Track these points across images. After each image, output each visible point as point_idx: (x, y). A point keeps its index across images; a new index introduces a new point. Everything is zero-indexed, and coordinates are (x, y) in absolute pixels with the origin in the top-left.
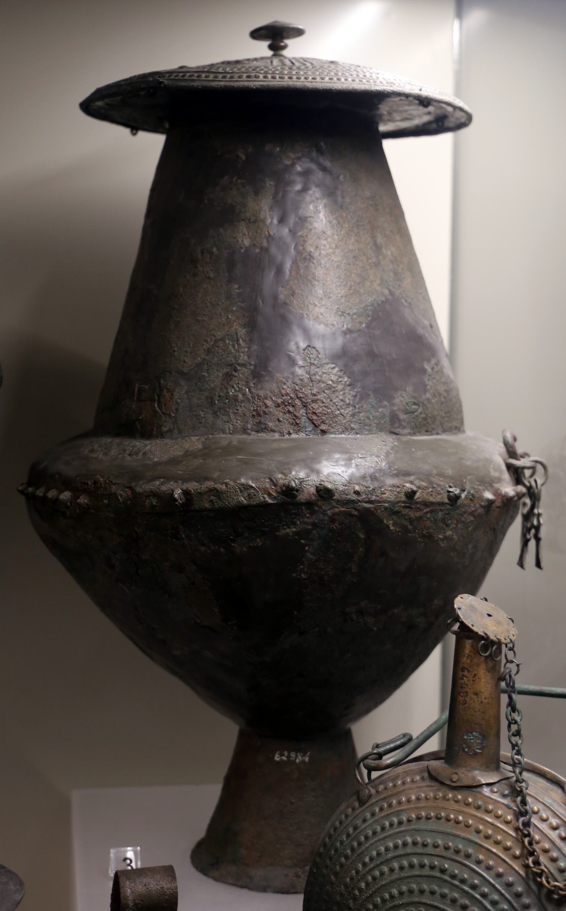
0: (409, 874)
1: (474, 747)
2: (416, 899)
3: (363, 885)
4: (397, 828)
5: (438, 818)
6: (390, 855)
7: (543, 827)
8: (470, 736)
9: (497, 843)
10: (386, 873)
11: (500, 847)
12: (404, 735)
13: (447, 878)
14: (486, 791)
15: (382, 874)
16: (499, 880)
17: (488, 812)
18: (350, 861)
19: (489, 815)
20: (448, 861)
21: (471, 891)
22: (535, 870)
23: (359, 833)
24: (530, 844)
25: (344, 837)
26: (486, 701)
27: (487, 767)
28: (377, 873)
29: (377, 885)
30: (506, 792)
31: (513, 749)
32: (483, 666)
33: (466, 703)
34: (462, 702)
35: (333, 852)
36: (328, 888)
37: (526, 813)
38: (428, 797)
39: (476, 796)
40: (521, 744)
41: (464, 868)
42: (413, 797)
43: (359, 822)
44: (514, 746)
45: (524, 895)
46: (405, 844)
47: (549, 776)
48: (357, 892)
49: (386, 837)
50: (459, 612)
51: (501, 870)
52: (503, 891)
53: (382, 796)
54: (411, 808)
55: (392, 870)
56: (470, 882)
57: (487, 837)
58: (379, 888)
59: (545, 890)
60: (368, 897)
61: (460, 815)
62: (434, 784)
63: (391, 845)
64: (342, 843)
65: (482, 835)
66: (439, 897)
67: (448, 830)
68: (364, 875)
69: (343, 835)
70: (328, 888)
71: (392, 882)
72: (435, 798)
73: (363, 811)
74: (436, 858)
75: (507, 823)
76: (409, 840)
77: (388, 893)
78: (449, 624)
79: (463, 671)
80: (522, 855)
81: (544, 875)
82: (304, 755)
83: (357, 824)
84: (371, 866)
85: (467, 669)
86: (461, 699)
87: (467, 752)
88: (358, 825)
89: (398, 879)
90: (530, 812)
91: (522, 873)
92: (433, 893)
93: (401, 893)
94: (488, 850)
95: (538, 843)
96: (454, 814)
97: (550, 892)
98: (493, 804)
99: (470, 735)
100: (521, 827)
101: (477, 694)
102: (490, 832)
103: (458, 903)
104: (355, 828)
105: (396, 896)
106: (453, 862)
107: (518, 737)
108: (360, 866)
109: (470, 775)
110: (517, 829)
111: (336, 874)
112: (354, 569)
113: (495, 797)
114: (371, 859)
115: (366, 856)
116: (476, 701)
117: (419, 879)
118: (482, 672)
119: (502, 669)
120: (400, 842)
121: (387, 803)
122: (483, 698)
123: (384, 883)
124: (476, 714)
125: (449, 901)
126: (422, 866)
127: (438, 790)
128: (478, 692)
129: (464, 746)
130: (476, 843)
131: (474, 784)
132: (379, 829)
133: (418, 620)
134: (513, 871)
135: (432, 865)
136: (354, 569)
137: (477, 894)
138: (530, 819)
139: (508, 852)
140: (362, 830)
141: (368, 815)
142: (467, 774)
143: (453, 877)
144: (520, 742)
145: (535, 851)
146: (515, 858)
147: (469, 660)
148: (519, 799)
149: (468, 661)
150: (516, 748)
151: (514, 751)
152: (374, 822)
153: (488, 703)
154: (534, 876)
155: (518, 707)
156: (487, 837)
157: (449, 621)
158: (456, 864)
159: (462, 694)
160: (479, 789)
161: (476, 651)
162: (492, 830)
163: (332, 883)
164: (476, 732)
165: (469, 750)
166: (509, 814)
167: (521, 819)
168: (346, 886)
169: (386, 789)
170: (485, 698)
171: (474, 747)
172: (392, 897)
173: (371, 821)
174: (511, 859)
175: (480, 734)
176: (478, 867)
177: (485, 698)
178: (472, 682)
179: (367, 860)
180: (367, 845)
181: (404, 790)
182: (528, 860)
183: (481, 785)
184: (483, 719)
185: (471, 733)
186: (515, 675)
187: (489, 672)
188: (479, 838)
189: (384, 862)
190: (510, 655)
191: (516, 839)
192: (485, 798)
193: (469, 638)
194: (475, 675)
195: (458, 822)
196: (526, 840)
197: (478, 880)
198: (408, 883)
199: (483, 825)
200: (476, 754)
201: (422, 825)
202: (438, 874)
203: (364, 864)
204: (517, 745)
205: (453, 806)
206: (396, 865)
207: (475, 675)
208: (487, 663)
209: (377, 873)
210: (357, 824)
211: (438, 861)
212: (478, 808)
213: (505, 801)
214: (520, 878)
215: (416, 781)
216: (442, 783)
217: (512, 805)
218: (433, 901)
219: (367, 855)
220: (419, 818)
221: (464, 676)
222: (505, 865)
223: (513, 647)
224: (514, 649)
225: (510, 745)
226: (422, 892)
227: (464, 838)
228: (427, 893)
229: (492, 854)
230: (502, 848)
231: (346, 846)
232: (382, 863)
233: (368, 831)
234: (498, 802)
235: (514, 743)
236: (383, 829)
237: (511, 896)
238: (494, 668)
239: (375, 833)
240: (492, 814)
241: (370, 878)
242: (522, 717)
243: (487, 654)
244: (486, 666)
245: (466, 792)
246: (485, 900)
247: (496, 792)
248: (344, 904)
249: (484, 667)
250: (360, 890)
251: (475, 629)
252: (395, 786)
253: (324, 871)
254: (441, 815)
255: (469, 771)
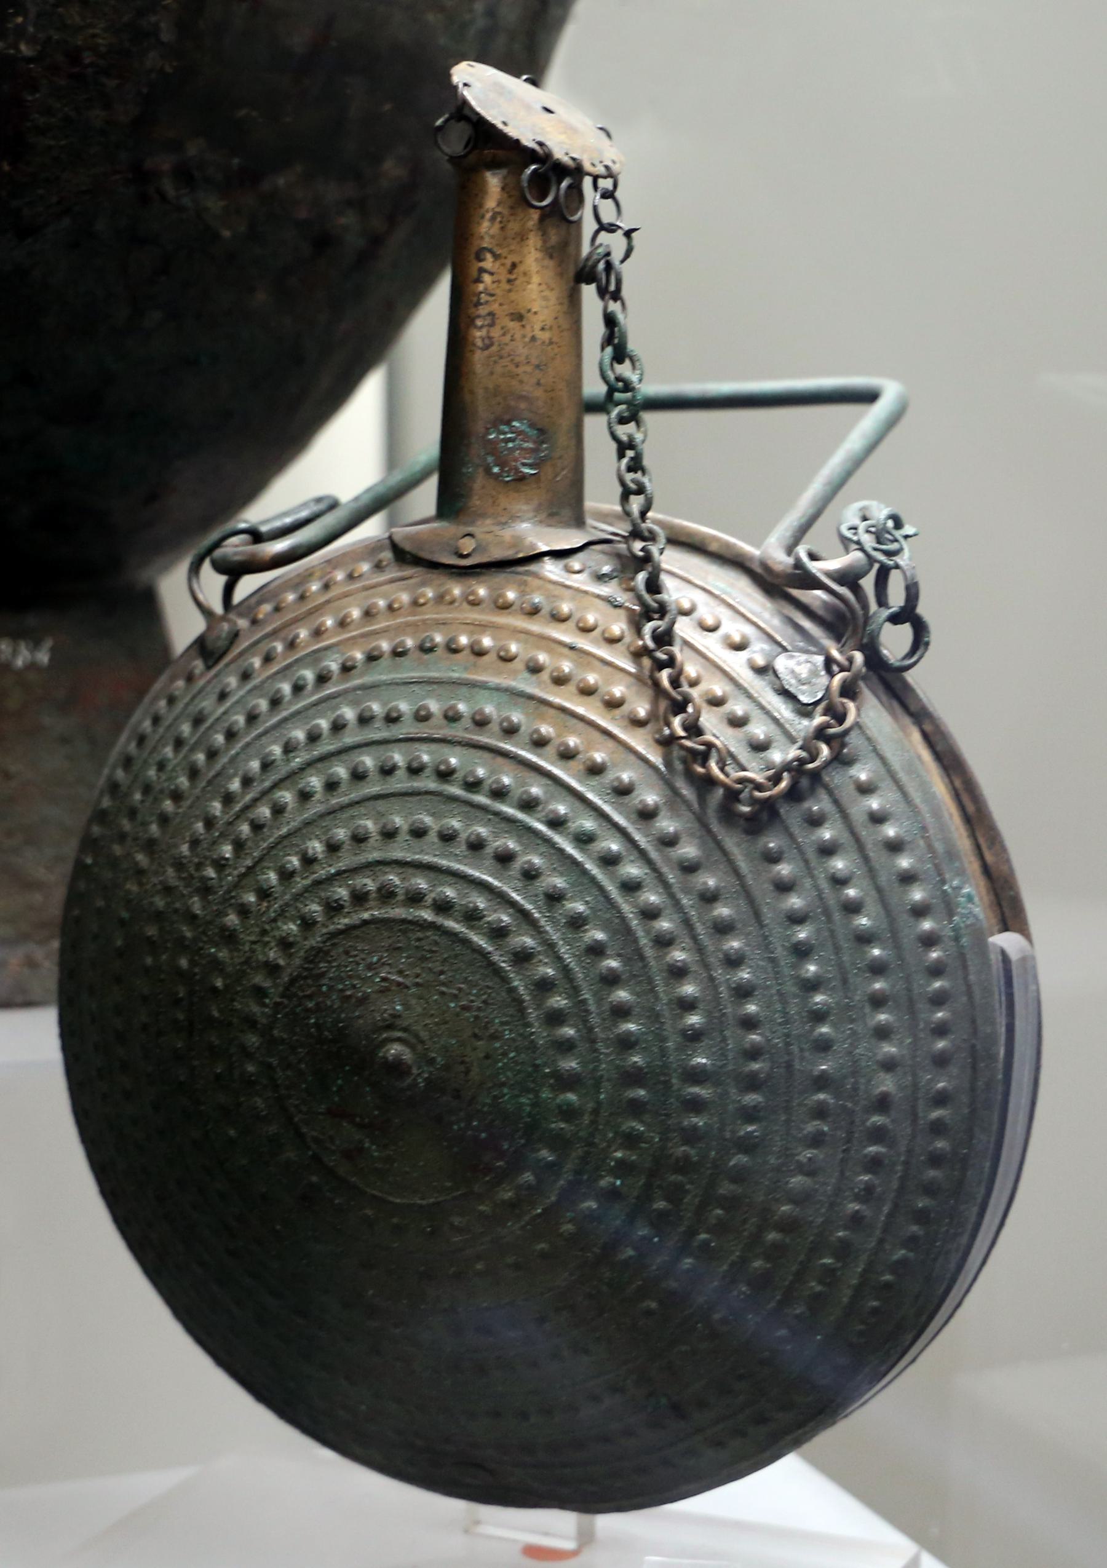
0: (354, 796)
1: (516, 460)
2: (375, 855)
3: (227, 851)
4: (312, 694)
5: (426, 649)
6: (297, 761)
7: (710, 644)
8: (505, 433)
9: (587, 692)
10: (289, 808)
11: (594, 701)
12: (319, 500)
13: (455, 790)
14: (551, 569)
15: (278, 810)
16: (595, 781)
17: (559, 619)
18: (186, 803)
19: (563, 626)
20: (458, 749)
21: (520, 815)
22: (688, 743)
23: (209, 728)
24: (675, 682)
25: (168, 751)
26: (545, 336)
27: (552, 515)
28: (264, 812)
29: (264, 840)
30: (606, 569)
31: (621, 455)
32: (534, 241)
33: (492, 344)
34: (479, 343)
35: (138, 796)
36: (132, 887)
37: (662, 610)
38: (396, 606)
39: (525, 583)
40: (643, 441)
41: (500, 760)
42: (356, 613)
43: (207, 703)
44: (623, 447)
45: (663, 813)
46: (338, 727)
47: (713, 547)
48: (211, 872)
49: (285, 720)
50: (467, 93)
51: (599, 757)
52: (607, 808)
53: (269, 629)
54: (353, 638)
55: (305, 796)
56: (517, 793)
57: (560, 681)
58: (271, 848)
59: (720, 792)
60: (242, 876)
61: (483, 632)
62: (409, 571)
63: (300, 735)
64: (161, 766)
65: (545, 676)
66: (436, 840)
67: (456, 675)
68: (230, 824)
69: (164, 746)
70: (132, 887)
71: (308, 824)
72: (415, 603)
73: (216, 676)
74: (424, 747)
75: (612, 641)
76: (349, 714)
77: (296, 854)
78: (440, 128)
79: (479, 258)
80: (653, 716)
81: (714, 755)
82: (36, 644)
83: (201, 712)
84: (248, 798)
85: (490, 251)
86: (478, 335)
87: (496, 477)
88: (206, 712)
89: (322, 816)
90: (672, 608)
91: (655, 757)
92: (419, 833)
93: (333, 848)
94: (563, 710)
95: (693, 684)
96: (471, 634)
97: (732, 795)
98: (573, 599)
99: (505, 428)
100: (651, 644)
101: (519, 317)
102: (566, 667)
103: (489, 850)
104: (198, 721)
105: (320, 856)
106: (472, 751)
107: (633, 424)
108: (216, 807)
109: (507, 534)
110: (638, 655)
111: (150, 846)
112: (167, 35)
113: (580, 581)
114: (247, 782)
115: (230, 778)
116: (518, 336)
117: (381, 805)
118: (532, 257)
119: (586, 249)
120: (324, 724)
121: (284, 640)
122: (537, 327)
123: (284, 830)
124: (520, 370)
125: (464, 847)
126: (388, 771)
127: (423, 584)
128: (523, 312)
129: (490, 459)
130: (531, 697)
131: (521, 555)
132: (263, 705)
133: (343, 221)
134: (632, 758)
135: (415, 765)
136: (167, 35)
137: (539, 820)
138: (673, 623)
139: (617, 712)
140: (218, 719)
141: (233, 681)
142: (500, 533)
143: (474, 785)
144: (639, 437)
145: (687, 700)
146: (637, 723)
147: (497, 226)
148: (641, 577)
149: (495, 229)
150: (630, 453)
151: (625, 461)
152: (250, 691)
153: (551, 343)
154: (689, 761)
155: (632, 346)
156: (560, 681)
157: (439, 122)
158: (480, 753)
159: (479, 323)
160: (533, 567)
161: (518, 200)
162: (573, 661)
163: (140, 872)
164: (520, 420)
165: (502, 470)
166: (616, 620)
167: (648, 628)
168: (179, 865)
169: (277, 609)
170: (543, 329)
171: (516, 460)
172: (308, 861)
173: (242, 693)
174: (624, 728)
175: (532, 425)
176: (539, 756)
177: (543, 329)
178: (507, 287)
179: (235, 785)
180: (233, 752)
181: (328, 602)
182: (668, 724)
183: (539, 557)
184: (538, 384)
185: (508, 423)
186: (622, 262)
187: (551, 257)
188: (539, 684)
189: (282, 780)
190: (608, 212)
191: (638, 678)
192: (551, 587)
193: (494, 165)
194: (514, 266)
195: (479, 652)
196: (664, 676)
197: (539, 785)
198: (353, 817)
199: (550, 651)
200: (522, 479)
201: (381, 674)
202: (432, 785)
203: (228, 799)
204: (631, 445)
205: (465, 615)
206: (315, 782)
207: (514, 266)
208: (544, 234)
209: (264, 812)
210: (201, 712)
211: (429, 753)
212: (534, 611)
213: (605, 590)
214: (650, 771)
215: (360, 576)
216: (434, 566)
217: (622, 597)
218: (421, 852)
219: (235, 775)
220: (372, 658)
221: (486, 271)
222: (611, 744)
223: (615, 186)
224: (618, 194)
225: (614, 446)
226: (389, 834)
227: (498, 689)
228: (404, 836)
229: (575, 721)
230: (599, 704)
231: (173, 770)
232: (276, 786)
233: (235, 717)
234: (586, 592)
235: (625, 438)
236: (276, 702)
237: (627, 818)
238: (562, 250)
239: (252, 718)
240: (571, 624)
241: (245, 829)
242: (641, 375)
243: (544, 203)
244: (545, 242)
245: (499, 578)
246: (560, 833)
247: (579, 572)
248: (176, 911)
249: (539, 244)
250: (221, 865)
251: (512, 132)
252: (302, 598)
253: (118, 850)
254: (432, 640)
255: (504, 524)
